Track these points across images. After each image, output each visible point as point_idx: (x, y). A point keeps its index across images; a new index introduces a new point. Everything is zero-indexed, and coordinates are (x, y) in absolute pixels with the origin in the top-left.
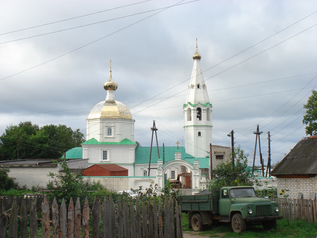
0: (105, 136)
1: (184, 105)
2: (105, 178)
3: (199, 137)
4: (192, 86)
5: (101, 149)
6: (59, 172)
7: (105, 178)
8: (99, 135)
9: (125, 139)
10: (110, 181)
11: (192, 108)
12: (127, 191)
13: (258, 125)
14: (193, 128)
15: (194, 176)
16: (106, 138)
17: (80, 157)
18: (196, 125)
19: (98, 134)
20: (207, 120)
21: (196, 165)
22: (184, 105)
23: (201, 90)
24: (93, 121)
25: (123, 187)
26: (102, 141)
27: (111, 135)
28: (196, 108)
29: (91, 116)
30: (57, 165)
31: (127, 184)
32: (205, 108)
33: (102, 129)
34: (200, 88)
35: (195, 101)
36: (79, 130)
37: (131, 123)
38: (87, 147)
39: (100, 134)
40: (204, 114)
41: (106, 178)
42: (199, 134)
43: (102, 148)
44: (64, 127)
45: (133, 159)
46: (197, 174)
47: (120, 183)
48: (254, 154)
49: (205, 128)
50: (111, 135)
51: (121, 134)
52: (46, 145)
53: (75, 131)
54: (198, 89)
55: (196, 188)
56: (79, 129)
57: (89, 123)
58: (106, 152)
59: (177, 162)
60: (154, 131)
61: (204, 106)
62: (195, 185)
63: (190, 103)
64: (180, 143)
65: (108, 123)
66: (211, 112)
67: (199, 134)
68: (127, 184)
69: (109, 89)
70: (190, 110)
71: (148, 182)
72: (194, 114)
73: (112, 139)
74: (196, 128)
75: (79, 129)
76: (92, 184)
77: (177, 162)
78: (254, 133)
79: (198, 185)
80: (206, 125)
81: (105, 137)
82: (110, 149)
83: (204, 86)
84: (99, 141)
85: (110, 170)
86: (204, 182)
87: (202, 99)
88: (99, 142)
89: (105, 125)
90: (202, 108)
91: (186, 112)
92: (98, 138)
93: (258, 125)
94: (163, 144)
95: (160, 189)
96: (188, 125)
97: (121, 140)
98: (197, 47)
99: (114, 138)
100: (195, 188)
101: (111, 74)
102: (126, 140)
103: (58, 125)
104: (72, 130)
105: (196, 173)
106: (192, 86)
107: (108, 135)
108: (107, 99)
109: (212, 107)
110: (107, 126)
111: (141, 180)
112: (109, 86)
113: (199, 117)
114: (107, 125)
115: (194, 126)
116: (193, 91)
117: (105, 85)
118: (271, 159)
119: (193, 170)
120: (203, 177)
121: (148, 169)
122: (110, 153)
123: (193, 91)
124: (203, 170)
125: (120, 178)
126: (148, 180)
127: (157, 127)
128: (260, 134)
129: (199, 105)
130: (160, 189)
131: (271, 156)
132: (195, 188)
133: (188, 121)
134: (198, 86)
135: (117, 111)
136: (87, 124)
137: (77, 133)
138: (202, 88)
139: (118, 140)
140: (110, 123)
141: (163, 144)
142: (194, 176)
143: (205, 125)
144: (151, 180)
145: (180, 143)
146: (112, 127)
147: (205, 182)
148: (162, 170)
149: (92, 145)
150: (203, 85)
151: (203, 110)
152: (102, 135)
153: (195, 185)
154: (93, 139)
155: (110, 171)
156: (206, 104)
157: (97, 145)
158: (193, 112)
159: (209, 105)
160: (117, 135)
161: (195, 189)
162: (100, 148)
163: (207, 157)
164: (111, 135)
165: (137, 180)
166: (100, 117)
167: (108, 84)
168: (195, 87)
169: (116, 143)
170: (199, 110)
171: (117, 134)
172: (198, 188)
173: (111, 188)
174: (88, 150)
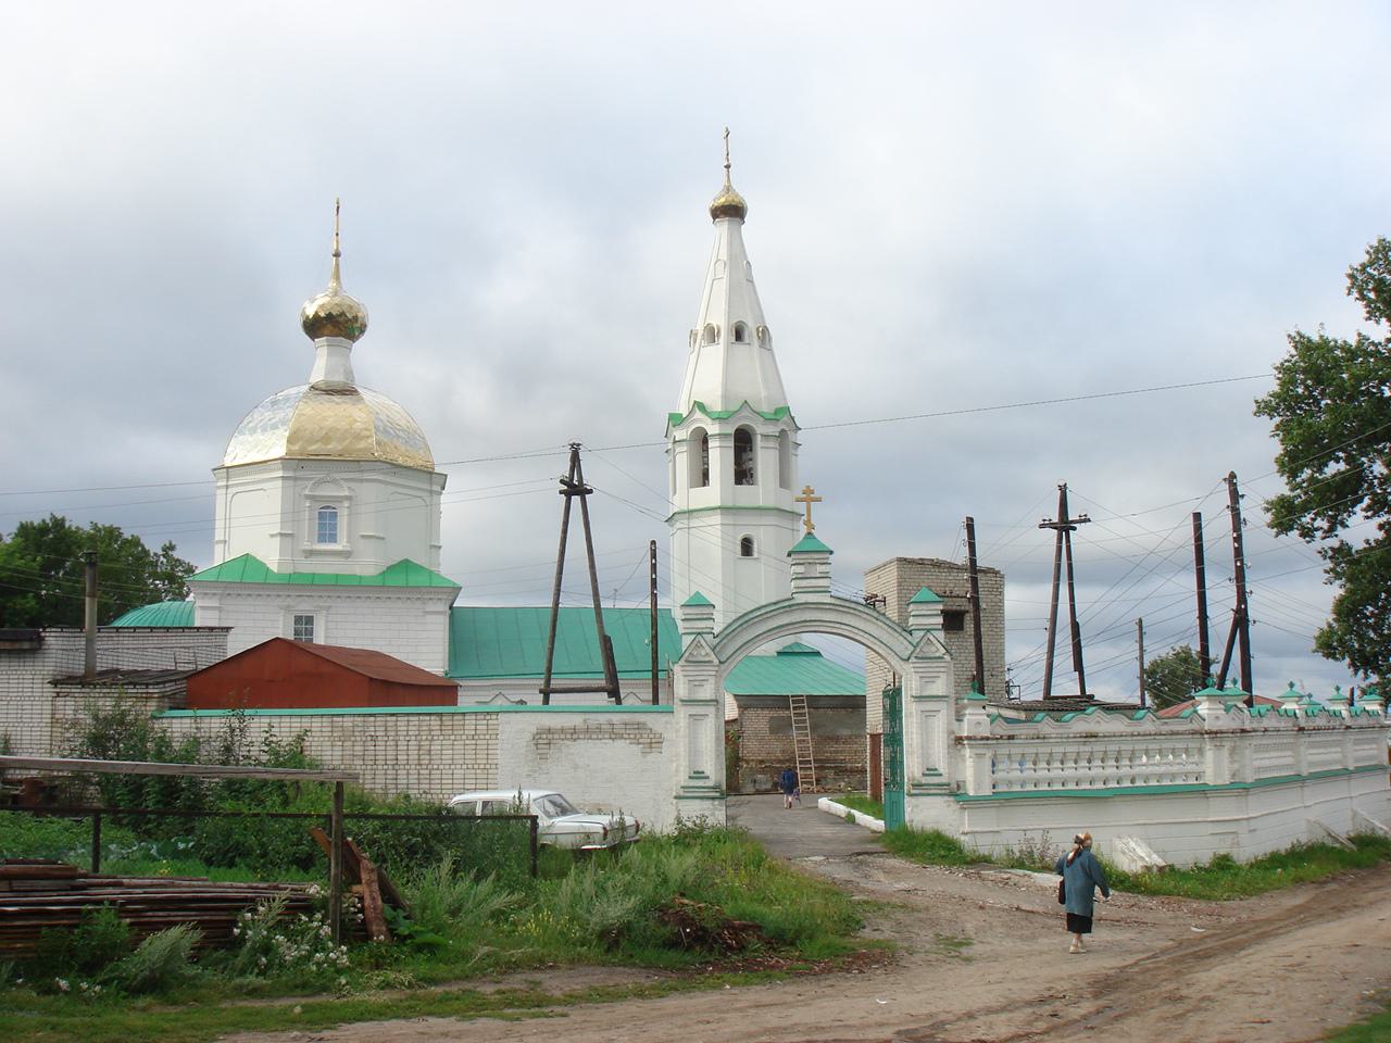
0: (307, 546)
1: (671, 417)
2: (343, 715)
3: (747, 561)
4: (712, 334)
5: (288, 609)
6: (55, 683)
7: (343, 715)
8: (278, 538)
9: (401, 562)
10: (374, 738)
11: (712, 429)
12: (525, 795)
13: (1065, 485)
14: (717, 519)
15: (920, 698)
16: (311, 553)
17: (185, 616)
18: (730, 504)
19: (272, 536)
20: (781, 486)
21: (928, 630)
22: (671, 417)
23: (749, 352)
24: (248, 474)
25: (459, 773)
26: (290, 570)
27: (333, 538)
28: (732, 431)
29: (241, 451)
30: (41, 640)
31: (482, 755)
32: (773, 430)
33: (290, 514)
34: (747, 340)
35: (725, 397)
36: (172, 548)
37: (426, 486)
38: (214, 594)
39: (281, 535)
40: (765, 459)
41: (348, 722)
42: (747, 547)
43: (289, 599)
44: (112, 533)
45: (440, 656)
46: (940, 687)
47: (436, 747)
48: (1048, 625)
49: (772, 519)
50: (336, 542)
51: (383, 539)
52: (23, 601)
53: (155, 554)
54: (739, 347)
55: (931, 771)
56: (170, 544)
57: (230, 483)
58: (310, 620)
59: (808, 615)
60: (576, 500)
61: (767, 420)
62: (925, 754)
63: (700, 406)
64: (819, 500)
65: (320, 482)
66: (793, 452)
67: (747, 547)
68: (482, 755)
69: (326, 332)
70: (703, 440)
71: (622, 738)
72: (720, 459)
73: (341, 560)
74: (730, 520)
75: (170, 544)
76: (254, 752)
77: (808, 615)
78: (1042, 526)
79: (940, 758)
80: (778, 506)
81: (305, 551)
82: (330, 607)
83: (764, 335)
84: (274, 568)
85: (370, 675)
86: (982, 739)
87: (756, 390)
88: (276, 571)
89: (307, 492)
90: (760, 429)
91: (685, 448)
92: (271, 556)
93: (1065, 485)
94: (653, 543)
95: (700, 783)
96: (691, 508)
97: (384, 564)
98: (728, 167)
99: (346, 554)
100: (924, 775)
101: (337, 265)
102: (406, 565)
103: (87, 528)
104: (143, 547)
105: (928, 679)
106: (712, 334)
107: (322, 539)
108: (318, 376)
109: (704, 485)
110: (312, 498)
111: (575, 730)
112: (329, 316)
113: (743, 475)
114: (316, 494)
115: (724, 509)
116: (715, 355)
117: (310, 313)
118: (1251, 615)
119: (913, 659)
120: (974, 706)
121: (541, 692)
122: (327, 629)
123: (715, 355)
124: (798, 702)
125: (441, 714)
126: (619, 729)
127: (589, 479)
128: (1074, 529)
129: (746, 413)
130: (700, 783)
131: (1250, 600)
132: (924, 775)
133: (691, 490)
134: (739, 335)
135: (366, 429)
136: (219, 492)
137: (162, 559)
138: (756, 343)
139: (367, 565)
140: (334, 481)
141: (653, 543)
142: (920, 698)
143: (771, 504)
144: (640, 726)
145: (819, 500)
146: (340, 499)
147: (988, 739)
148: (716, 662)
149: (242, 584)
150: (758, 329)
151: (765, 436)
152: (290, 539)
153: (925, 754)
154: (247, 558)
155: (371, 679)
156: (775, 413)
157: (264, 585)
158: (718, 444)
159: (785, 418)
160: (362, 541)
161: (924, 780)
162: (278, 602)
163: (779, 653)
164: (333, 538)
165: (549, 731)
166: (280, 450)
167: (322, 306)
168: (725, 336)
169: (360, 577)
170: (743, 441)
171: (363, 536)
172: (941, 771)
173: (380, 780)
174: (219, 609)
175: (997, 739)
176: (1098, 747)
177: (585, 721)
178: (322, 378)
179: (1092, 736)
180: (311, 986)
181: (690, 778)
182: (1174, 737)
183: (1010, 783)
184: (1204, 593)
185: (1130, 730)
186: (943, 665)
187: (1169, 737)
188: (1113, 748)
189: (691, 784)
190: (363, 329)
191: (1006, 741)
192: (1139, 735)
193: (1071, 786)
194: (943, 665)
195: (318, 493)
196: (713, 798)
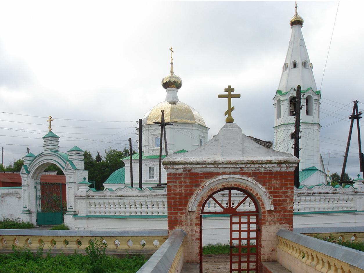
34: (307, 67)
37: (192, 128)
134: (295, 66)
175: (139, 196)
176: (126, 201)
177: (8, 191)
178: (171, 100)
179: (122, 196)
180: (213, 257)
181: (24, 207)
182: (156, 197)
183: (110, 212)
184: (348, 141)
185: (139, 194)
186: (71, 172)
187: (153, 197)
188: (132, 201)
189: (24, 209)
190: (299, 85)
191: (92, 198)
192: (140, 196)
193: (117, 214)
194: (71, 172)
195: (155, 133)
196: (27, 213)
